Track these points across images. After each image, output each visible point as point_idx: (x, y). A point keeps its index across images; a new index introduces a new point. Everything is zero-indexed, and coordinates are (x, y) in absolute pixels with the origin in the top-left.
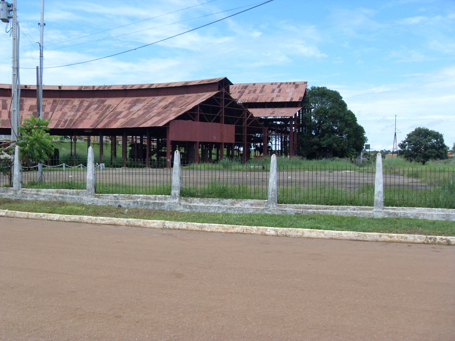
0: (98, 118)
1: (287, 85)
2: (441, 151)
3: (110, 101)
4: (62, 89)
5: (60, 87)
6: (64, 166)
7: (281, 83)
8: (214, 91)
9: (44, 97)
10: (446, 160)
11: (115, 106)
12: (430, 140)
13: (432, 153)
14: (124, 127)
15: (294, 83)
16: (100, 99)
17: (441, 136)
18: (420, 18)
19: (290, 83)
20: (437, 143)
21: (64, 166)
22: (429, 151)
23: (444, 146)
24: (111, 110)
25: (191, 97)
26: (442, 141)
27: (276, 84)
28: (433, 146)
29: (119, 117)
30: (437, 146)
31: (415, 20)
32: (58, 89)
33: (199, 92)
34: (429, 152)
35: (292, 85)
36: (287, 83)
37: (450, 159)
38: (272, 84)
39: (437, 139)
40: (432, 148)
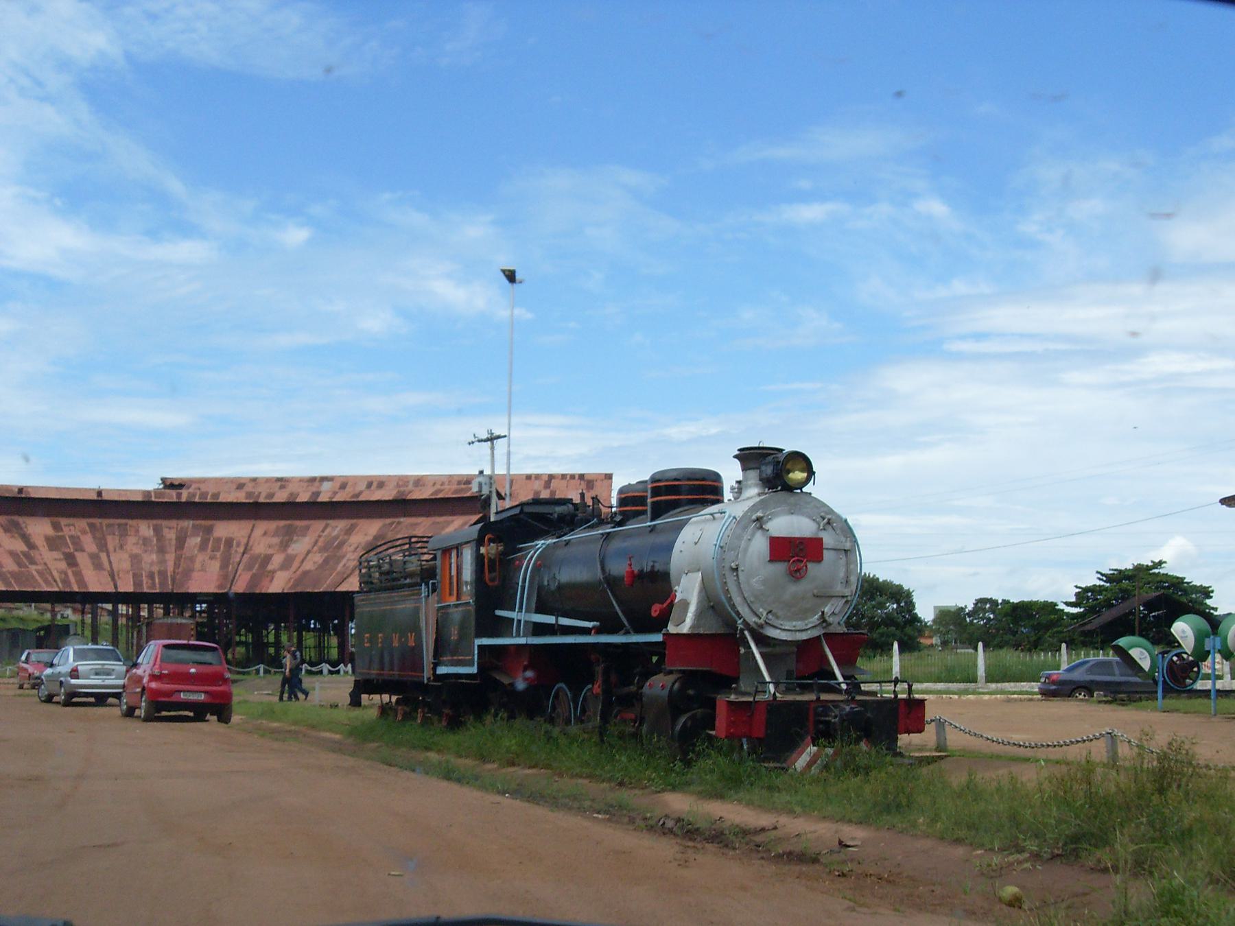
0: (221, 568)
1: (564, 482)
2: (908, 630)
3: (224, 529)
4: (106, 497)
5: (99, 493)
6: (262, 671)
7: (551, 477)
8: (475, 514)
9: (1217, 697)
10: (916, 654)
11: (245, 541)
12: (881, 606)
13: (888, 636)
14: (299, 590)
15: (582, 477)
16: (198, 522)
17: (908, 595)
18: (830, 207)
19: (572, 477)
20: (900, 610)
21: (262, 671)
22: (880, 631)
23: (915, 619)
24: (241, 550)
25: (417, 524)
26: (910, 605)
27: (538, 477)
28: (889, 621)
29: (270, 567)
30: (900, 620)
31: (811, 213)
32: (94, 497)
33: (434, 515)
34: (882, 635)
35: (576, 481)
36: (564, 476)
37: (926, 652)
38: (529, 477)
39: (898, 603)
40: (887, 626)
